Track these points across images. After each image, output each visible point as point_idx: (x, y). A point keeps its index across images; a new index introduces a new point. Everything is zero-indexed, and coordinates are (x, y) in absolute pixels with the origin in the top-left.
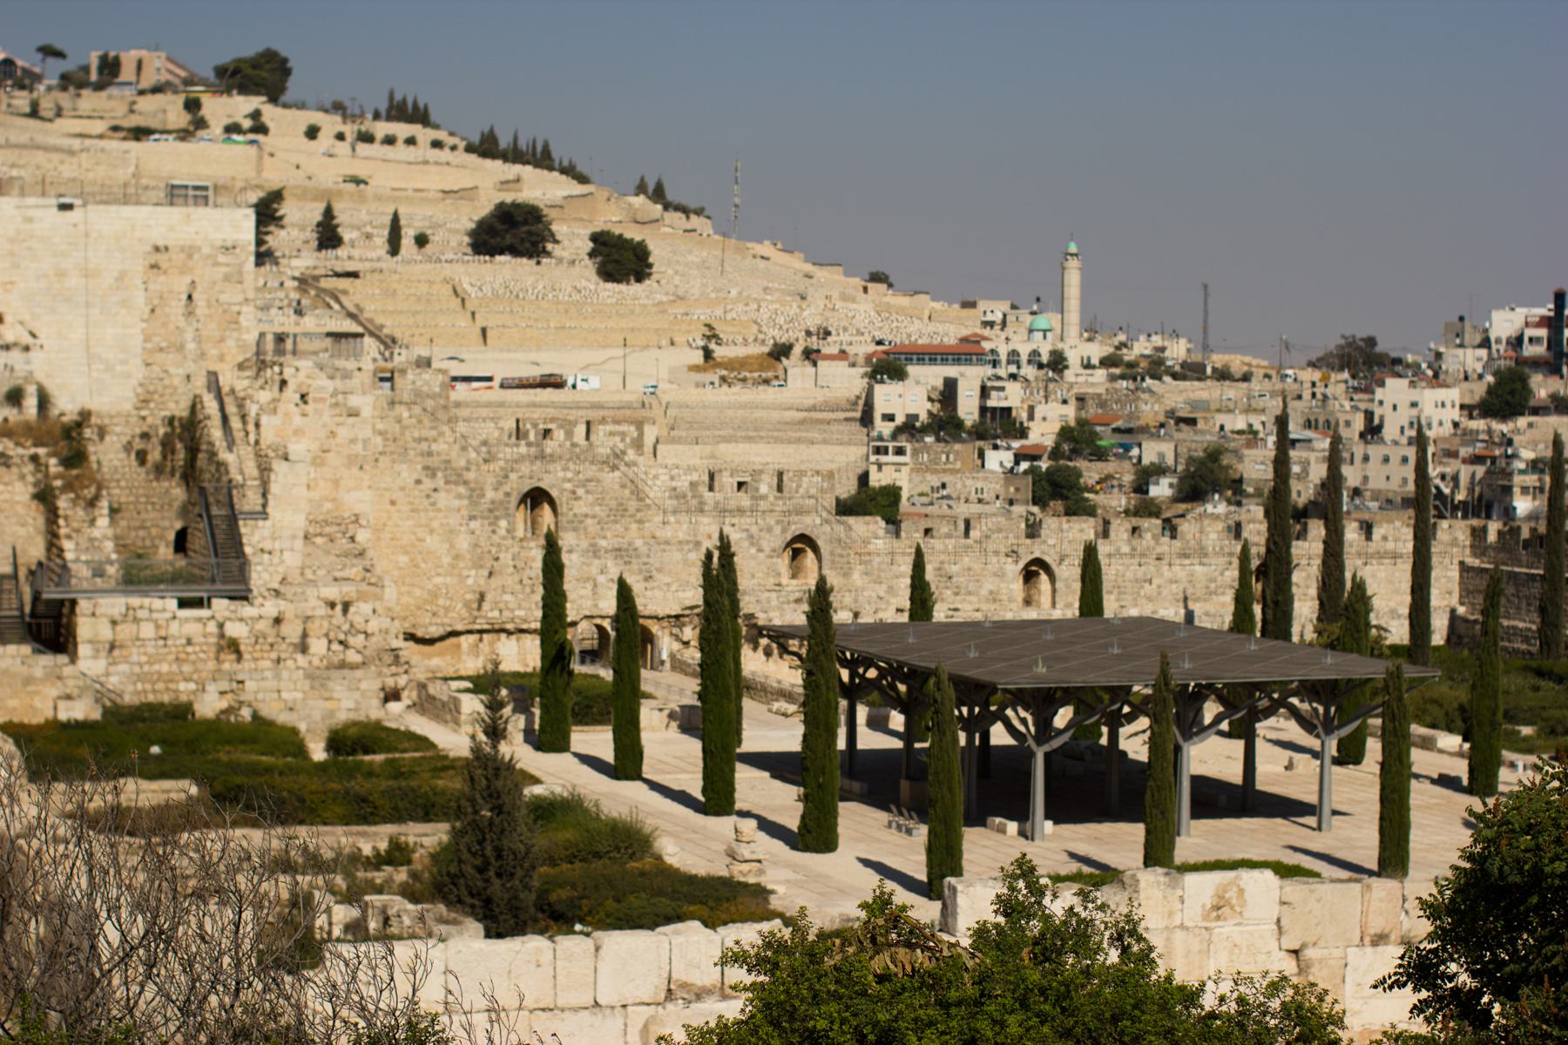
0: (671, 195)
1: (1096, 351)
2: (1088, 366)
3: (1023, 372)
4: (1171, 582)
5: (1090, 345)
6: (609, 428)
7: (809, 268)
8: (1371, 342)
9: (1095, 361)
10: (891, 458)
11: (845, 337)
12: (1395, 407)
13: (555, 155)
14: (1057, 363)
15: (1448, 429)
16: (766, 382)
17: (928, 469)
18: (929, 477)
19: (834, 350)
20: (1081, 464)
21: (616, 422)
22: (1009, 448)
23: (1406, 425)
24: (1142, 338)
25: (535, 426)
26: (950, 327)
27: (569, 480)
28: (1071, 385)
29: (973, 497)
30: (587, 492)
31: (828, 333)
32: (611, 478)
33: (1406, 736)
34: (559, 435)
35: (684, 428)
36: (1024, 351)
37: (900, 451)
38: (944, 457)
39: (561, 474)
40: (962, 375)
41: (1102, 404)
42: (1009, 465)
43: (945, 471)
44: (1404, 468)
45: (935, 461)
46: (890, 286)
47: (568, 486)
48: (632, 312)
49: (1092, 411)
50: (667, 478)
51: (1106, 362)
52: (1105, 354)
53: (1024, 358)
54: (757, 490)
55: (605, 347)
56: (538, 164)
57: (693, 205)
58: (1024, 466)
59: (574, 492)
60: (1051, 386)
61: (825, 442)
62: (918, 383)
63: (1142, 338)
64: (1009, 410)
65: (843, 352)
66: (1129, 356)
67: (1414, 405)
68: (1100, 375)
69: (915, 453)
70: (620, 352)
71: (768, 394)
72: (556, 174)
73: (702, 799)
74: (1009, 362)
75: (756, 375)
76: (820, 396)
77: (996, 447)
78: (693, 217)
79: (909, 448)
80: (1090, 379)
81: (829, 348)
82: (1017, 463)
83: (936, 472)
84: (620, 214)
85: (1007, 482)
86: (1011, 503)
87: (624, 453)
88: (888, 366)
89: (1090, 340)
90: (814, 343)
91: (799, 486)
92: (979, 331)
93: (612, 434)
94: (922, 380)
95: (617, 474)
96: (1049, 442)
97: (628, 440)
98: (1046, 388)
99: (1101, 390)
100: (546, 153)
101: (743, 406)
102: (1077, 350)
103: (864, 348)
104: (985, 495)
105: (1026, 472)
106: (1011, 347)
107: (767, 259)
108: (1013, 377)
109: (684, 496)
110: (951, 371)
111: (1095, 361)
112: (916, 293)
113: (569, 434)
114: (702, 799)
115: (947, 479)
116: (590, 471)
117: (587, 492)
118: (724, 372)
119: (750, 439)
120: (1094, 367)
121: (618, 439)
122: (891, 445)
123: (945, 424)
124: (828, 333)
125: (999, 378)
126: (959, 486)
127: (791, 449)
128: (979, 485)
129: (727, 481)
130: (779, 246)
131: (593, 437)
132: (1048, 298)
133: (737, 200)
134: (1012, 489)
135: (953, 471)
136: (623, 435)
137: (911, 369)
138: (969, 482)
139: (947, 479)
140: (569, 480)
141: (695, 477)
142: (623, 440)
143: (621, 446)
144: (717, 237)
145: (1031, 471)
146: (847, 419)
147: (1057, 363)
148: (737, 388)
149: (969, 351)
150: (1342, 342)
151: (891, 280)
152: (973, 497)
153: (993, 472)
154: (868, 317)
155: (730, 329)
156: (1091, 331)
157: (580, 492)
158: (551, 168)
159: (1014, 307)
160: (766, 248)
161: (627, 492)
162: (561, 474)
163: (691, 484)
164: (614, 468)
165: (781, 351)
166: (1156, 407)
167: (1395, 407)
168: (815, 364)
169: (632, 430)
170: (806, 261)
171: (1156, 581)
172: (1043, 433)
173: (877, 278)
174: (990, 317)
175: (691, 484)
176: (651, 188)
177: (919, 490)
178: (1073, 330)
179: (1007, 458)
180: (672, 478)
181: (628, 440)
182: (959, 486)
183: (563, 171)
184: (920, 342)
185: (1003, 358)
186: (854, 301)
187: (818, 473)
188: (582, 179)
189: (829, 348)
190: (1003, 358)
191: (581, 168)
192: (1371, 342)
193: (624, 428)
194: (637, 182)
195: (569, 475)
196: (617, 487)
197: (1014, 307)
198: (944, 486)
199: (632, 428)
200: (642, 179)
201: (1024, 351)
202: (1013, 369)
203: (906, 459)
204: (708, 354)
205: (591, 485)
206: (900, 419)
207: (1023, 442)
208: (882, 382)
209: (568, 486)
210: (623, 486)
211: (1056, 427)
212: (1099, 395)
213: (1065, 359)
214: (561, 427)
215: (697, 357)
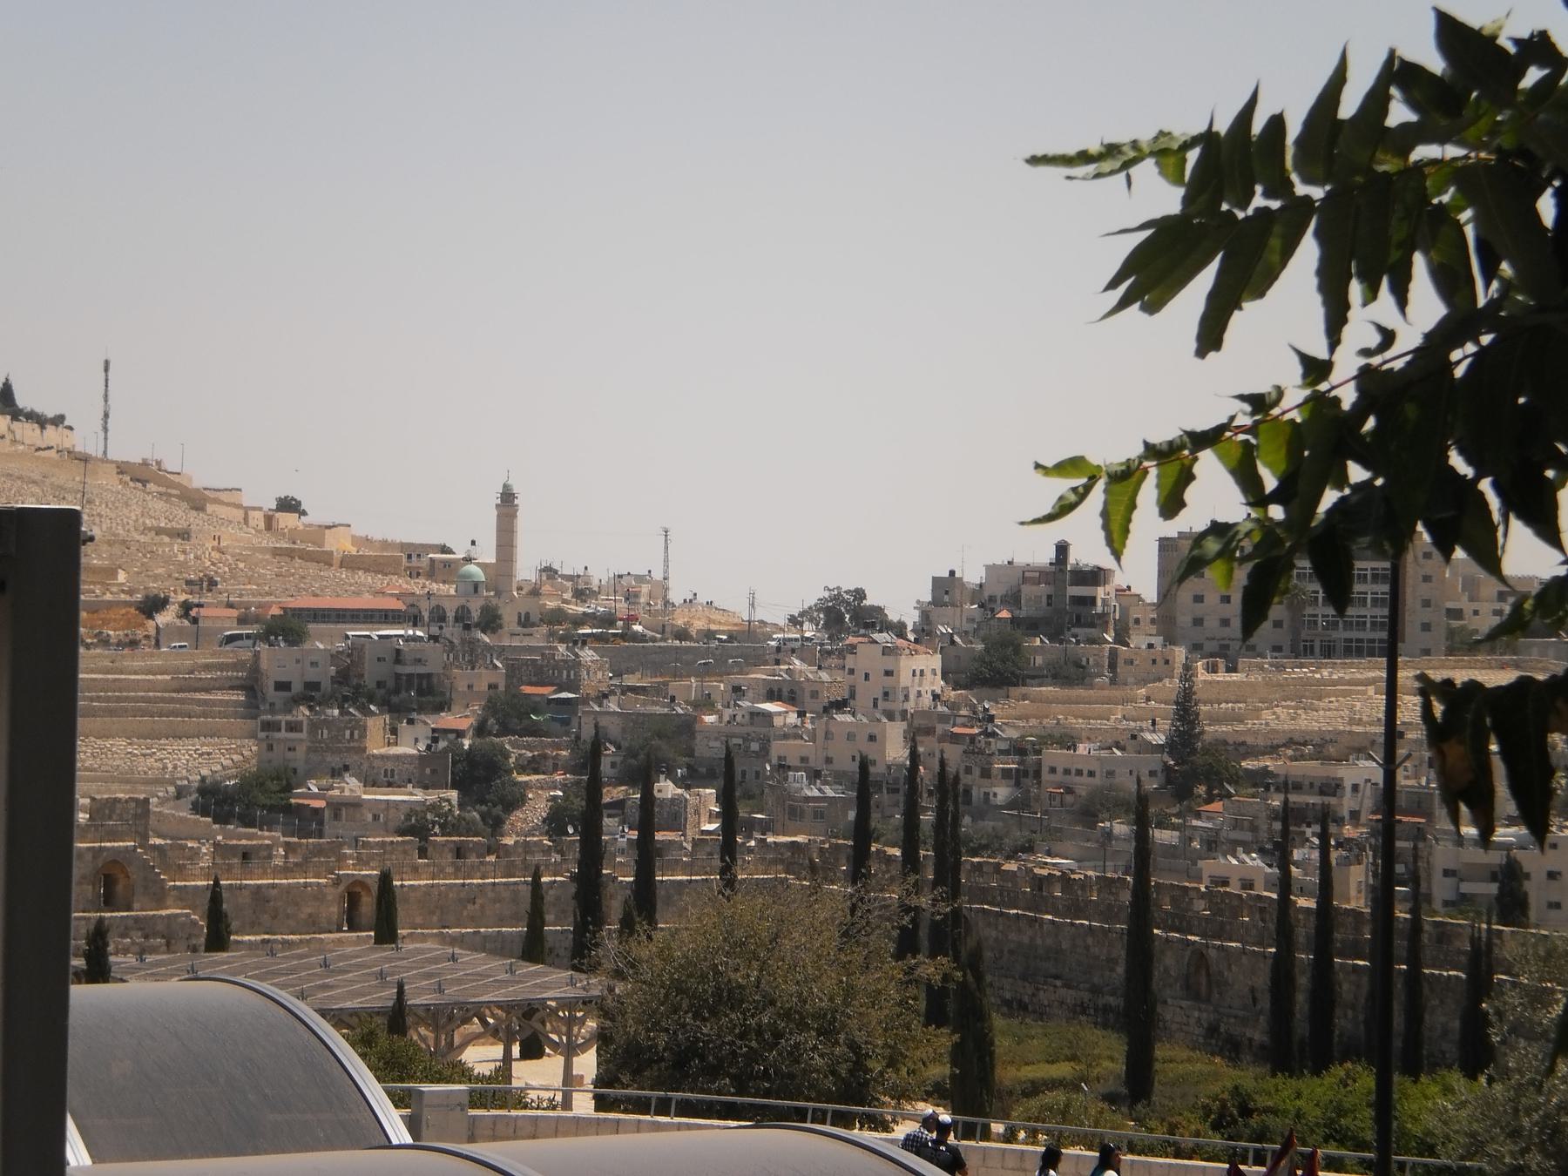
4: (495, 901)
8: (860, 594)
12: (867, 676)
15: (927, 700)
20: (506, 742)
23: (880, 696)
33: (1378, 1149)
38: (348, 733)
43: (349, 750)
44: (1216, 624)
64: (429, 676)
67: (888, 673)
73: (1546, 72)
78: (50, 429)
83: (339, 751)
114: (1546, 72)
119: (111, 713)
120: (533, 625)
134: (428, 771)
150: (826, 594)
167: (867, 676)
171: (479, 901)
192: (860, 594)
206: (297, 687)
213: (499, 617)
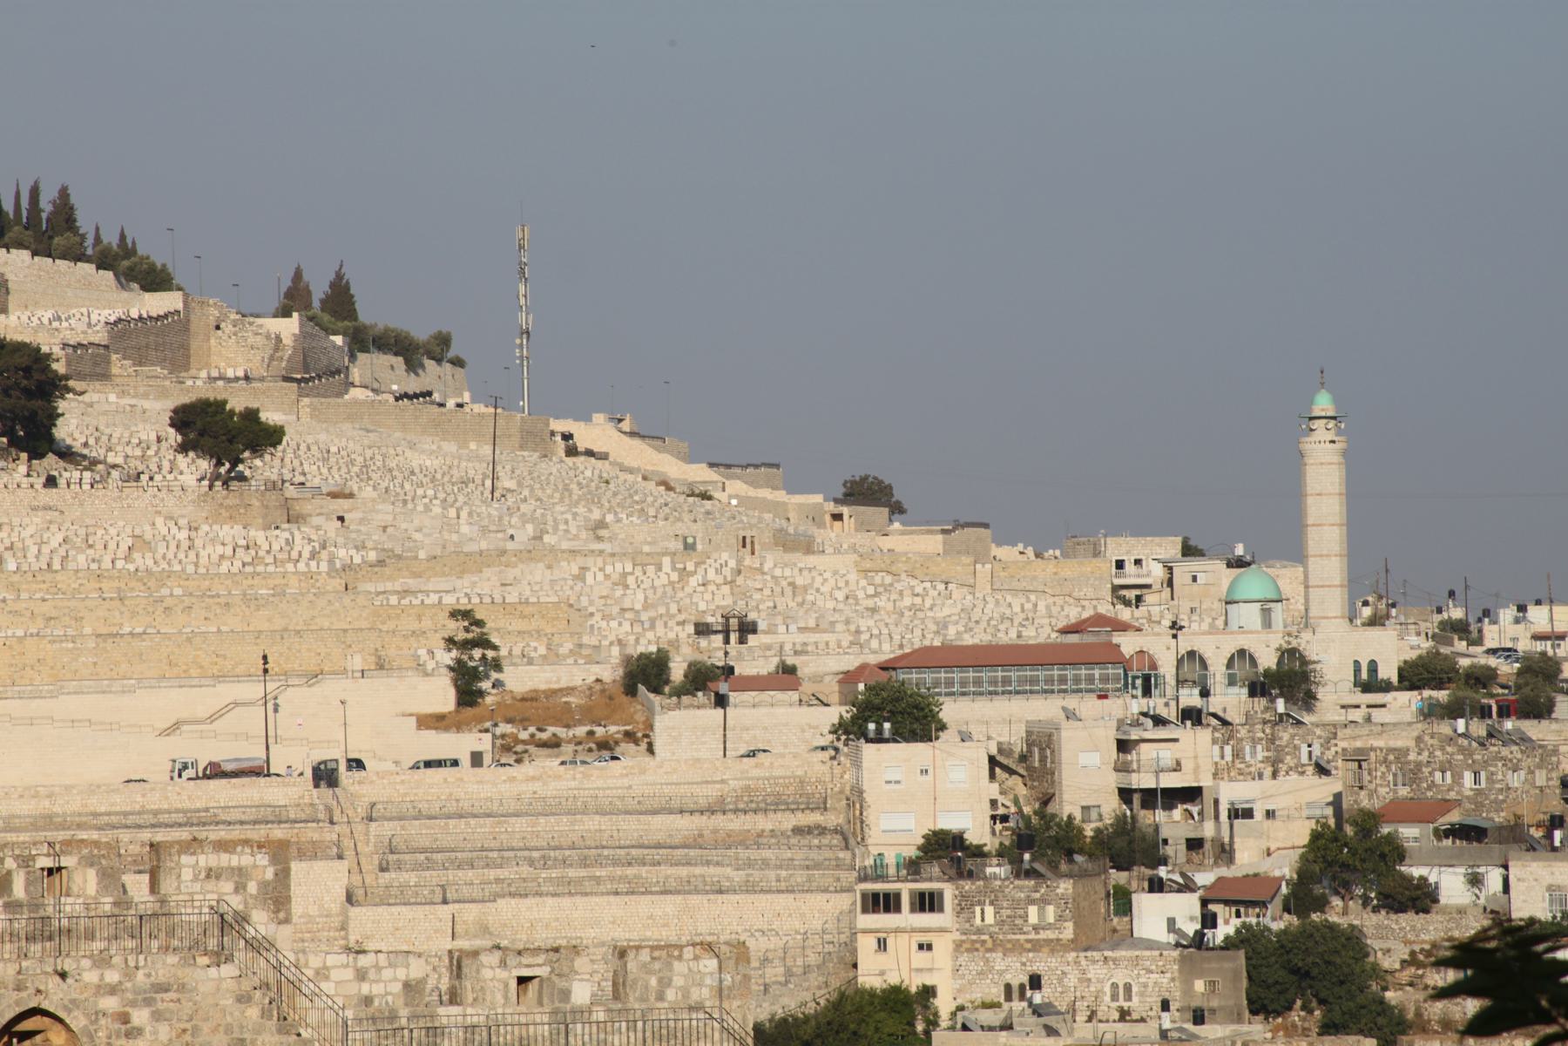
0: (370, 313)
1: (1392, 648)
2: (1370, 683)
3: (1215, 704)
5: (1375, 632)
6: (207, 859)
7: (700, 473)
9: (1388, 672)
10: (907, 918)
11: (789, 638)
13: (85, 223)
14: (1289, 682)
16: (606, 747)
17: (997, 945)
18: (999, 961)
19: (764, 666)
21: (223, 846)
22: (1187, 887)
24: (1507, 614)
25: (26, 862)
26: (1025, 595)
27: (113, 990)
28: (1333, 731)
29: (1108, 1008)
30: (157, 1016)
31: (747, 629)
32: (215, 982)
34: (86, 882)
35: (403, 863)
36: (1217, 653)
37: (927, 902)
39: (91, 977)
40: (1070, 715)
41: (1413, 775)
42: (1191, 928)
43: (1036, 946)
45: (1013, 922)
46: (897, 509)
47: (110, 1003)
48: (280, 593)
49: (1381, 792)
50: (349, 974)
51: (1414, 676)
52: (1412, 655)
53: (1217, 668)
54: (566, 995)
55: (220, 677)
56: (42, 247)
57: (421, 332)
58: (1226, 928)
59: (124, 1018)
60: (1285, 734)
61: (750, 888)
62: (965, 737)
63: (1507, 614)
65: (789, 671)
66: (1467, 657)
68: (1405, 703)
69: (965, 906)
70: (254, 690)
71: (624, 775)
72: (88, 268)
74: (1180, 682)
75: (581, 731)
76: (737, 776)
77: (1157, 886)
79: (949, 892)
80: (1378, 715)
81: (752, 661)
82: (1209, 921)
84: (238, 357)
85: (1188, 970)
86: (1199, 1017)
87: (243, 918)
88: (892, 708)
89: (1375, 621)
90: (713, 650)
91: (665, 983)
92: (1105, 609)
93: (211, 874)
94: (977, 731)
95: (228, 970)
96: (1284, 868)
97: (252, 887)
98: (1272, 740)
99: (1404, 740)
100: (65, 215)
101: (550, 809)
102: (1337, 650)
103: (827, 663)
104: (1135, 1002)
105: (1229, 944)
106: (1185, 644)
107: (603, 457)
108: (1192, 716)
109: (393, 1017)
110: (1043, 709)
111: (1388, 672)
112: (959, 525)
113: (109, 878)
115: (1042, 964)
116: (166, 966)
117: (157, 1016)
118: (505, 728)
120: (1386, 687)
121: (227, 887)
122: (906, 890)
123: (1041, 843)
124: (747, 629)
125: (1159, 721)
126: (1072, 980)
127: (670, 905)
128: (1121, 977)
129: (494, 976)
130: (626, 426)
131: (167, 885)
132: (1257, 530)
133: (523, 319)
134: (1199, 986)
135: (1055, 946)
136: (240, 877)
137: (950, 711)
138: (1096, 972)
139: (1042, 964)
140: (113, 990)
141: (416, 969)
142: (240, 888)
143: (236, 902)
144: (479, 408)
145: (1242, 940)
146: (798, 831)
147: (1289, 682)
148: (546, 764)
149: (1084, 656)
151: (898, 495)
152: (1108, 1008)
153: (1150, 945)
154: (856, 593)
155: (517, 625)
156: (1375, 596)
157: (140, 1017)
158: (79, 257)
159: (1189, 551)
160: (594, 432)
161: (253, 1013)
162: (91, 977)
163: (407, 985)
164: (221, 957)
165: (647, 674)
166: (1541, 778)
168: (721, 701)
169: (262, 866)
170: (690, 459)
172: (1272, 849)
173: (865, 493)
174: (1131, 575)
175: (407, 985)
176: (319, 289)
177: (978, 996)
178: (1331, 602)
179: (1185, 909)
180: (361, 975)
181: (252, 887)
182: (1072, 980)
183: (104, 261)
184: (968, 640)
185: (1167, 669)
186: (809, 547)
187: (709, 947)
188: (154, 279)
189: (752, 661)
190: (1167, 669)
191: (152, 249)
193: (243, 859)
194: (287, 283)
195: (112, 977)
196: (228, 1001)
197: (1189, 551)
198: (1035, 982)
199: (262, 859)
200: (298, 275)
201: (1217, 653)
202: (1191, 698)
203: (943, 919)
204: (468, 694)
205: (164, 1001)
207: (1224, 872)
208: (879, 739)
209: (110, 1003)
210: (243, 999)
211: (1300, 834)
212: (1401, 753)
214: (90, 862)
215: (442, 696)
